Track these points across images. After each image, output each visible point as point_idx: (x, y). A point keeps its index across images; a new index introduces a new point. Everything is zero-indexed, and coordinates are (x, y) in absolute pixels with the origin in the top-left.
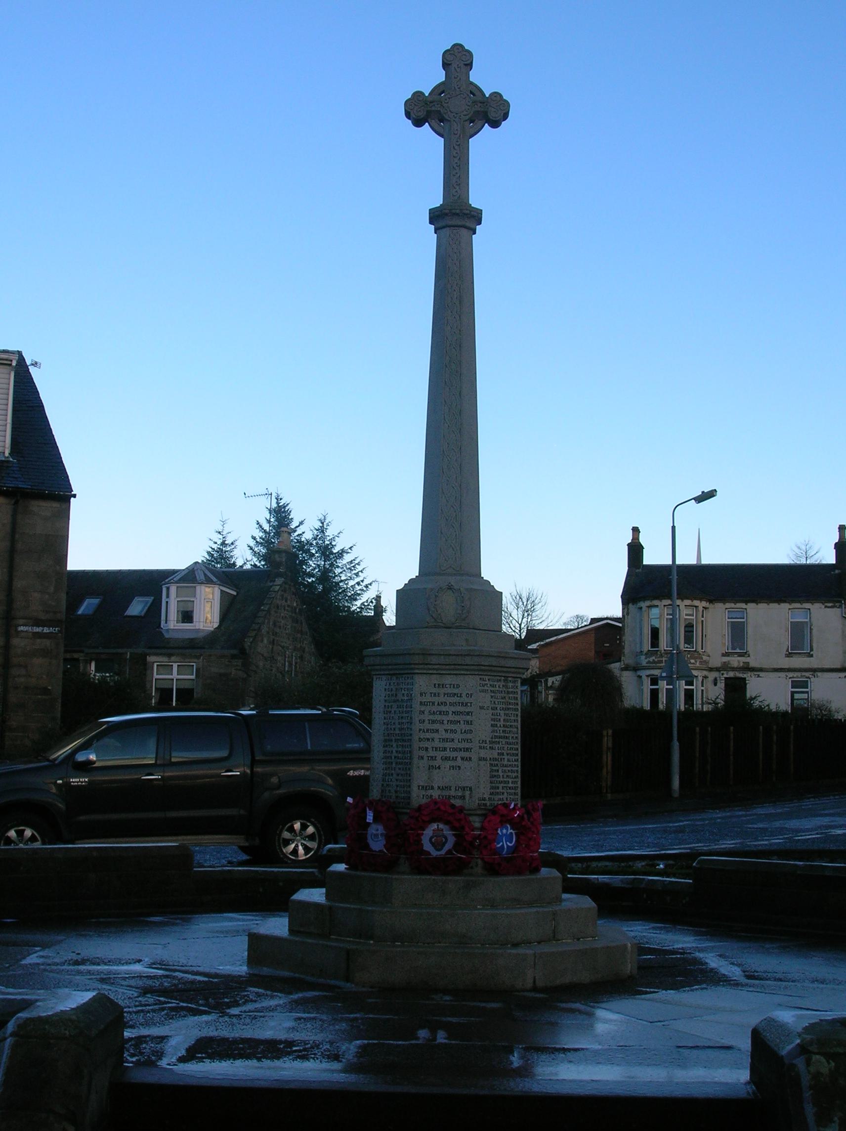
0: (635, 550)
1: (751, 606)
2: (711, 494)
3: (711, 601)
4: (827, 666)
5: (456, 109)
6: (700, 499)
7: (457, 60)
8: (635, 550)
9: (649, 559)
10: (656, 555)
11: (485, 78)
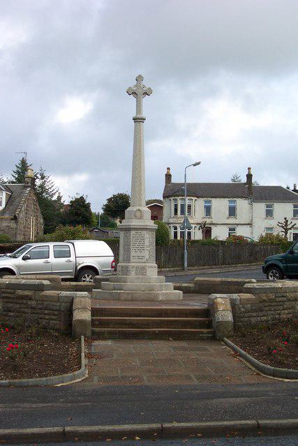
0: (168, 177)
1: (213, 200)
2: (199, 163)
3: (198, 197)
4: (243, 223)
5: (139, 92)
6: (195, 165)
7: (139, 79)
8: (168, 177)
9: (174, 180)
10: (177, 179)
11: (146, 83)
